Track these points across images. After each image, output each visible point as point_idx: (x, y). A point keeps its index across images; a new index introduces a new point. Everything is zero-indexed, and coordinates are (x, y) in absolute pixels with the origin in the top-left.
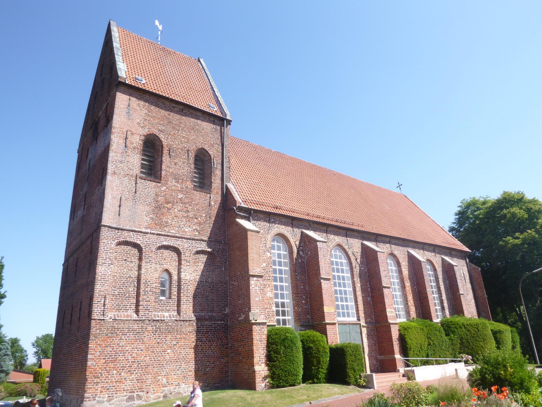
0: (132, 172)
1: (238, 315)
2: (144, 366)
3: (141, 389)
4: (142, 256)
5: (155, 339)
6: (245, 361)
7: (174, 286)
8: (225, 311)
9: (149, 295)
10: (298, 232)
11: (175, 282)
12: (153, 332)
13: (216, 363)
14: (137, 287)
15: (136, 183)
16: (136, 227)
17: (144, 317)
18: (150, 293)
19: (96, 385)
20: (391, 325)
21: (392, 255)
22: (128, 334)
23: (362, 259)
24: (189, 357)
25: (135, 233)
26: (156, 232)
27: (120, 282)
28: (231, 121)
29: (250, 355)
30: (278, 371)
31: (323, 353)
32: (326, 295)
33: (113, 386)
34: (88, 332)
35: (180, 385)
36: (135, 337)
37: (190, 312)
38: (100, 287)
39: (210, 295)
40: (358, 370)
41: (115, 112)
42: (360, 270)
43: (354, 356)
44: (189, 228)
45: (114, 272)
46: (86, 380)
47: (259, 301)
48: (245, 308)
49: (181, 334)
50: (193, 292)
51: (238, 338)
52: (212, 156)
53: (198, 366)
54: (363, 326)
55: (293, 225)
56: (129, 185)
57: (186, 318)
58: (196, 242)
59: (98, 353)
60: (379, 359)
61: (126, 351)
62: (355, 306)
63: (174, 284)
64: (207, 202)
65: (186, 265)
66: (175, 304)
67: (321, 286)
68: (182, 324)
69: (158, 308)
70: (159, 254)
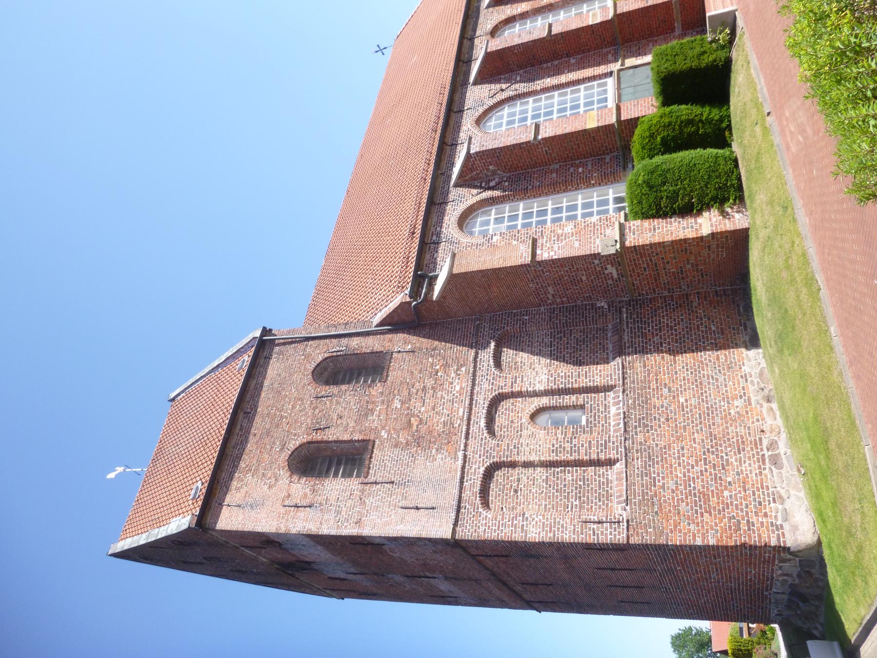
0: (355, 492)
1: (609, 279)
2: (711, 441)
3: (756, 444)
4: (507, 462)
5: (660, 426)
6: (693, 258)
7: (561, 401)
8: (603, 307)
9: (579, 444)
10: (454, 193)
11: (553, 400)
13: (700, 313)
14: (565, 466)
15: (376, 483)
16: (453, 478)
17: (620, 449)
18: (575, 441)
19: (753, 525)
20: (618, 12)
21: (494, 33)
22: (653, 475)
23: (502, 81)
24: (691, 364)
25: (466, 478)
26: (463, 441)
27: (557, 498)
28: (264, 329)
29: (681, 246)
30: (710, 192)
31: (672, 116)
32: (565, 128)
33: (754, 494)
34: (652, 548)
35: (745, 374)
36: (658, 463)
37: (608, 369)
38: (567, 532)
39: (574, 337)
40: (702, 47)
41: (251, 530)
42: (521, 81)
43: (677, 58)
45: (539, 509)
46: (743, 545)
47: (580, 241)
48: (594, 266)
49: (649, 381)
50: (570, 367)
51: (651, 277)
52: (326, 355)
53: (708, 345)
54: (623, 64)
55: (443, 203)
56: (379, 495)
57: (619, 374)
58: (480, 368)
59: (692, 527)
60: (680, 32)
61: (685, 476)
62: (587, 83)
63: (556, 402)
65: (522, 382)
66: (595, 397)
67: (549, 138)
68: (630, 380)
69: (603, 426)
70: (502, 433)
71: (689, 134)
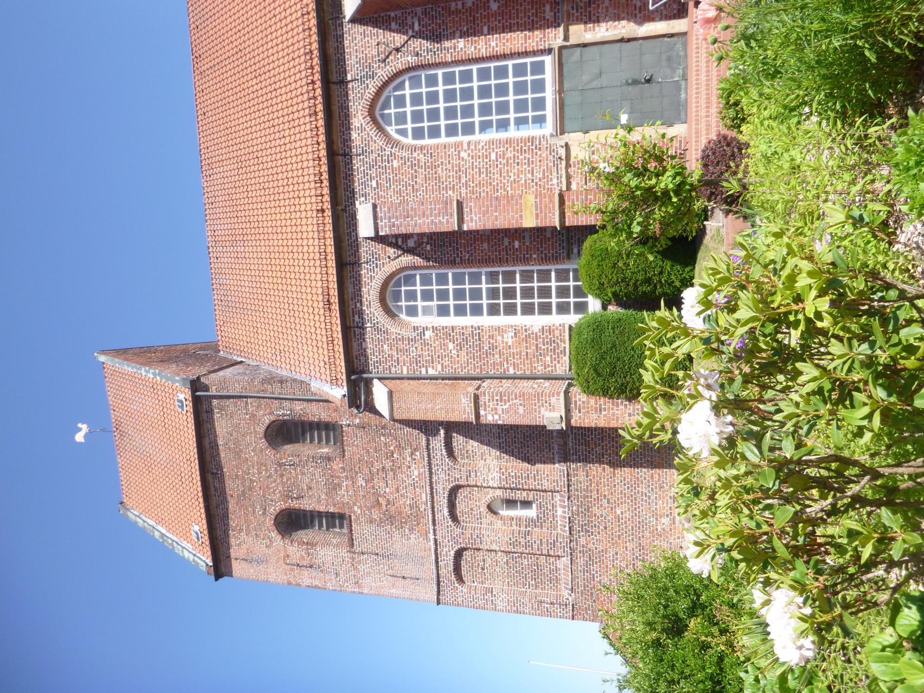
2: (640, 551)
5: (599, 533)
12: (589, 536)
26: (431, 527)
44: (412, 468)
53: (645, 463)
54: (566, 38)
57: (564, 481)
58: (434, 457)
64: (360, 433)
65: (476, 477)
71: (644, 293)
